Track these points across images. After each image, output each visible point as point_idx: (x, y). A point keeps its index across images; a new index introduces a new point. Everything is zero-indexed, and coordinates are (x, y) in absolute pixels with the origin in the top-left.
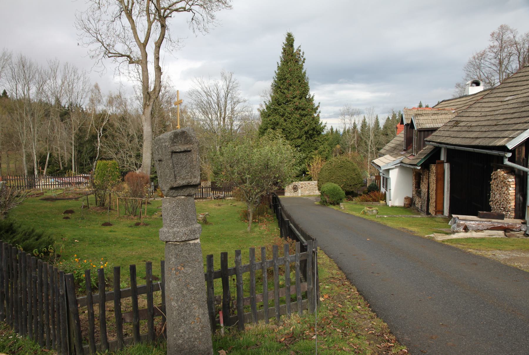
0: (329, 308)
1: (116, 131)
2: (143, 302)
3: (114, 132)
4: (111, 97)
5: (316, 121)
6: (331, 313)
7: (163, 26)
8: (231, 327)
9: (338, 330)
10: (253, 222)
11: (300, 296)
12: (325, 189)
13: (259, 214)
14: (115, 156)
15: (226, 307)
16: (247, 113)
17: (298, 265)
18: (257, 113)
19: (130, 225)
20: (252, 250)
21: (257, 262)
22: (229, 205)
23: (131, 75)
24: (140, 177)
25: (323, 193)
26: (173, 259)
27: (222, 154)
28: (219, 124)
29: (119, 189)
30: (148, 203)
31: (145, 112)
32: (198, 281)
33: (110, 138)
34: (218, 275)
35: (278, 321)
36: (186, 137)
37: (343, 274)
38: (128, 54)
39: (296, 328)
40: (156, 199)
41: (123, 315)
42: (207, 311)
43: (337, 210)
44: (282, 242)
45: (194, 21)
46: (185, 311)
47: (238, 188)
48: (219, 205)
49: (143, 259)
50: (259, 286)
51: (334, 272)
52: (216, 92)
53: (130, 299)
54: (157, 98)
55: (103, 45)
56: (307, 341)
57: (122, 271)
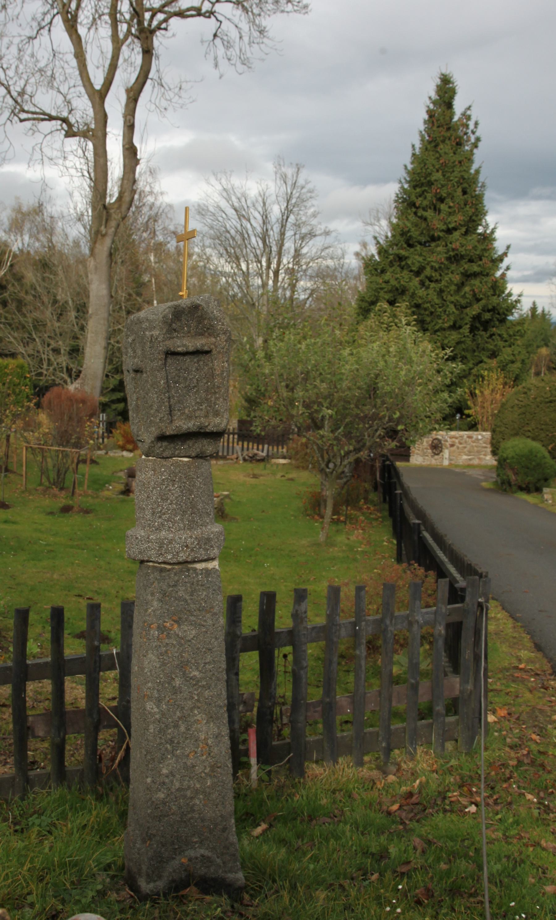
0: (508, 740)
1: (27, 293)
2: (75, 691)
3: (22, 294)
4: (18, 210)
5: (498, 287)
6: (513, 754)
7: (148, 52)
8: (273, 768)
9: (529, 796)
10: (333, 521)
11: (440, 708)
12: (509, 453)
13: (347, 503)
14: (21, 349)
15: (265, 719)
16: (330, 263)
17: (440, 635)
18: (352, 262)
19: (49, 510)
20: (334, 592)
21: (344, 620)
22: (278, 476)
23: (68, 163)
24: (77, 400)
25: (502, 463)
26: (155, 603)
27: (269, 357)
28: (264, 285)
29: (30, 426)
30: (93, 462)
31: (96, 251)
32: (209, 658)
33: (12, 306)
34: (250, 644)
35: (386, 763)
36: (201, 319)
37: (545, 661)
38: (65, 114)
39: (428, 782)
40: (111, 454)
41: (30, 719)
42: (225, 731)
43: (535, 505)
44: (408, 575)
45: (218, 41)
46: (176, 726)
47: (304, 440)
48: (255, 476)
49: (76, 592)
50: (341, 674)
51: (524, 654)
52: (260, 209)
53: (47, 685)
54: (123, 218)
55: (9, 92)
56: (454, 817)
57: (32, 617)
